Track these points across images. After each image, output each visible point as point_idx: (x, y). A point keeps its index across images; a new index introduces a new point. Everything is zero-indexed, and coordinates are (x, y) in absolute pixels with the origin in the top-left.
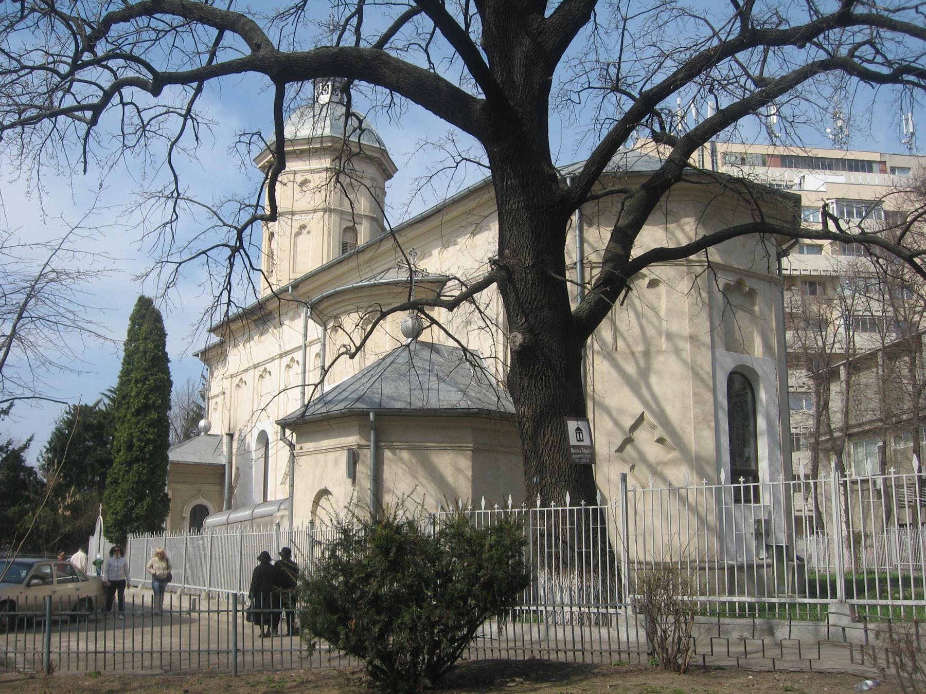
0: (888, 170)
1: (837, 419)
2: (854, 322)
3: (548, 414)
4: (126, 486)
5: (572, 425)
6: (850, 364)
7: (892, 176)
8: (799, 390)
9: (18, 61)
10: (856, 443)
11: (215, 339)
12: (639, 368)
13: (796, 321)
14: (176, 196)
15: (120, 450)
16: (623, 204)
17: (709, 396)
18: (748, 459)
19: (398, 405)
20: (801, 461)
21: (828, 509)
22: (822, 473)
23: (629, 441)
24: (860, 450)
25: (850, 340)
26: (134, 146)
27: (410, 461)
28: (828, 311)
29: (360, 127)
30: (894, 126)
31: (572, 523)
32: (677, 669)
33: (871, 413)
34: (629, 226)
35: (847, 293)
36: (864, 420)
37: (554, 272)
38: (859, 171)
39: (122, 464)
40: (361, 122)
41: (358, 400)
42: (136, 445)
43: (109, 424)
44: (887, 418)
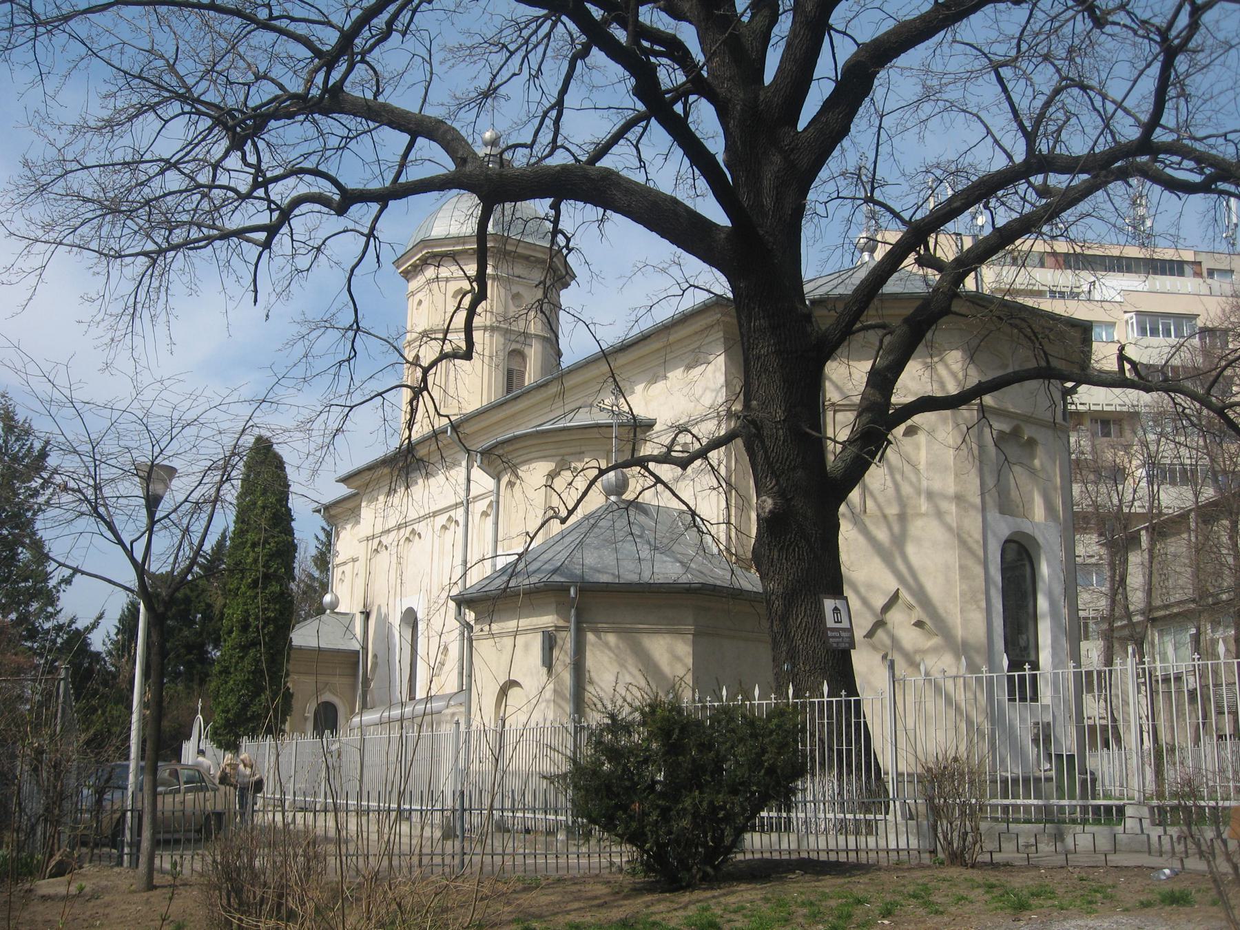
0: (1205, 274)
1: (1137, 599)
2: (1159, 473)
3: (801, 590)
4: (240, 677)
5: (829, 604)
6: (1154, 529)
7: (1209, 281)
8: (1089, 561)
9: (192, 179)
10: (1162, 630)
11: (344, 490)
12: (892, 534)
13: (1084, 473)
14: (356, 328)
15: (231, 632)
16: (881, 342)
17: (979, 570)
18: (1026, 648)
19: (604, 578)
20: (1092, 652)
21: (1126, 716)
22: (1117, 661)
23: (880, 624)
24: (1166, 638)
25: (1153, 497)
26: (308, 270)
27: (618, 647)
28: (1126, 460)
29: (567, 246)
30: (1206, 241)
31: (830, 717)
32: (964, 864)
33: (1181, 591)
34: (888, 368)
35: (1151, 437)
36: (1172, 600)
37: (810, 428)
38: (1166, 274)
39: (235, 649)
40: (568, 240)
41: (555, 571)
42: (253, 625)
43: (197, 597)
44: (1201, 598)
